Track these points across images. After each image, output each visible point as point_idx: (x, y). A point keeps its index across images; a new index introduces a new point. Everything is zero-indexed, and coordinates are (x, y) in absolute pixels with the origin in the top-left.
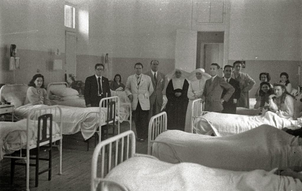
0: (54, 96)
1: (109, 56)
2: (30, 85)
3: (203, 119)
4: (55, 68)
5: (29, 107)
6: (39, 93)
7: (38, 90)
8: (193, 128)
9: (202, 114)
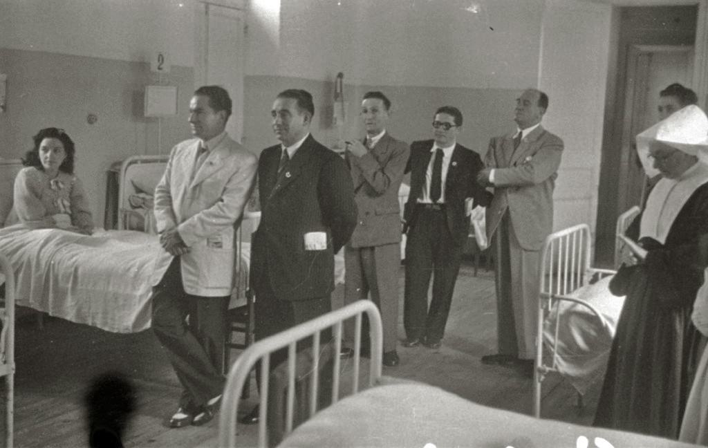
0: (142, 195)
1: (344, 81)
2: (26, 163)
3: (580, 308)
4: (150, 111)
5: (12, 236)
6: (54, 187)
7: (50, 180)
8: (544, 336)
9: (591, 278)
